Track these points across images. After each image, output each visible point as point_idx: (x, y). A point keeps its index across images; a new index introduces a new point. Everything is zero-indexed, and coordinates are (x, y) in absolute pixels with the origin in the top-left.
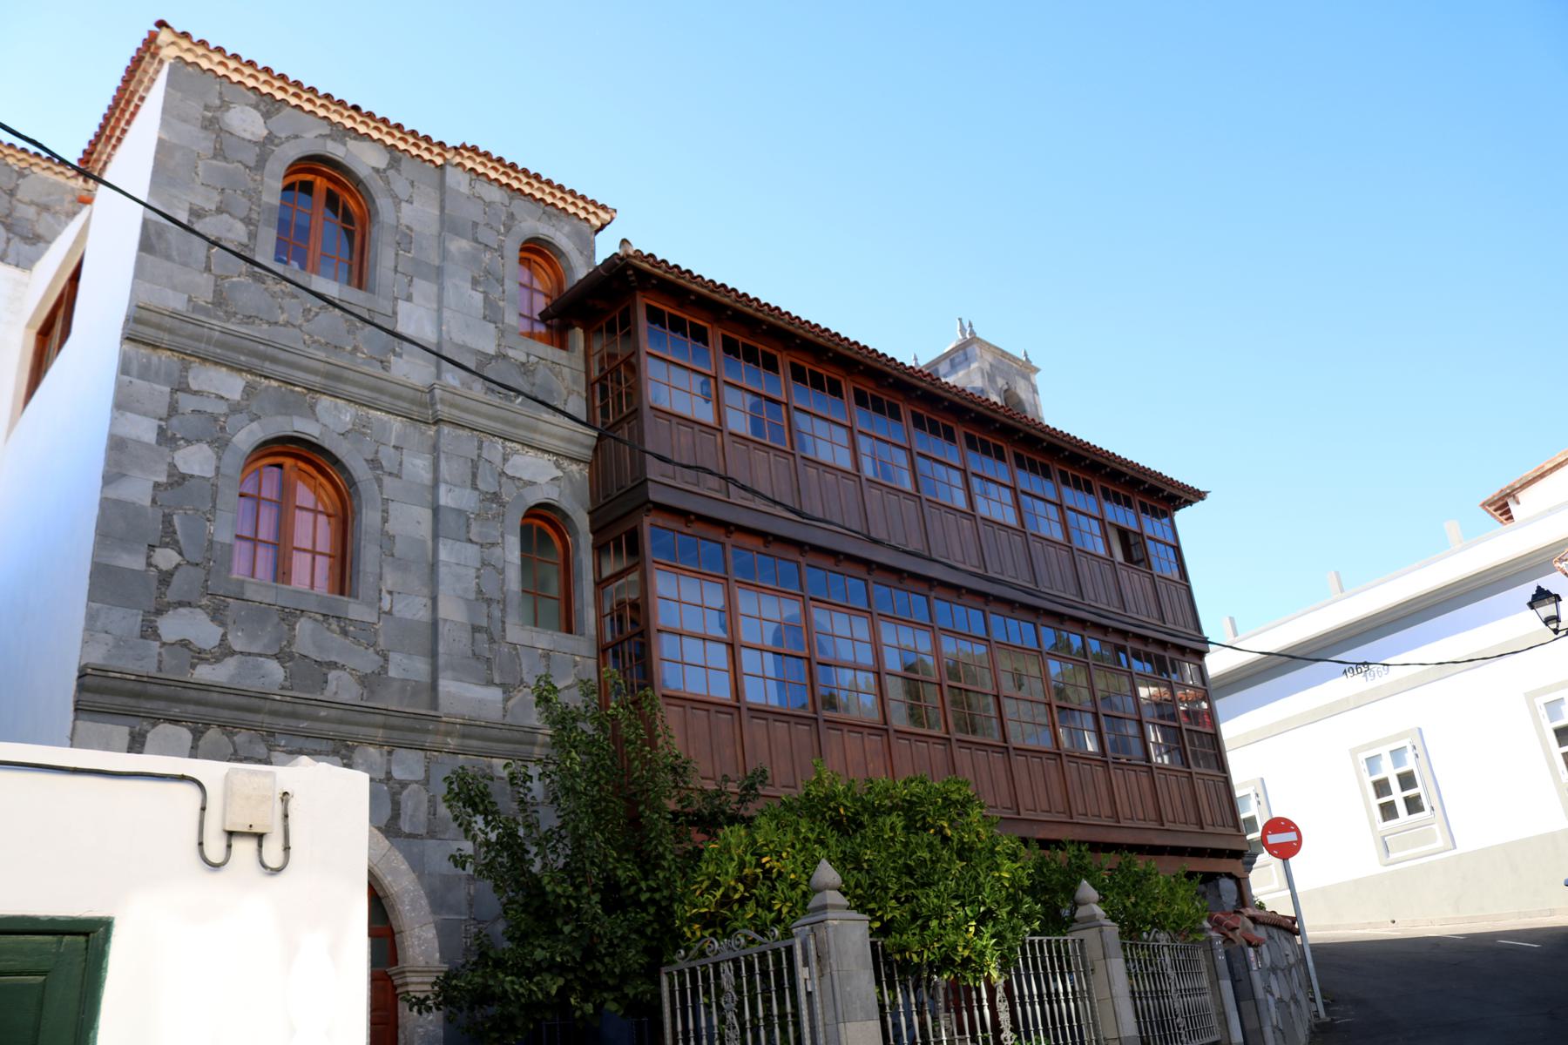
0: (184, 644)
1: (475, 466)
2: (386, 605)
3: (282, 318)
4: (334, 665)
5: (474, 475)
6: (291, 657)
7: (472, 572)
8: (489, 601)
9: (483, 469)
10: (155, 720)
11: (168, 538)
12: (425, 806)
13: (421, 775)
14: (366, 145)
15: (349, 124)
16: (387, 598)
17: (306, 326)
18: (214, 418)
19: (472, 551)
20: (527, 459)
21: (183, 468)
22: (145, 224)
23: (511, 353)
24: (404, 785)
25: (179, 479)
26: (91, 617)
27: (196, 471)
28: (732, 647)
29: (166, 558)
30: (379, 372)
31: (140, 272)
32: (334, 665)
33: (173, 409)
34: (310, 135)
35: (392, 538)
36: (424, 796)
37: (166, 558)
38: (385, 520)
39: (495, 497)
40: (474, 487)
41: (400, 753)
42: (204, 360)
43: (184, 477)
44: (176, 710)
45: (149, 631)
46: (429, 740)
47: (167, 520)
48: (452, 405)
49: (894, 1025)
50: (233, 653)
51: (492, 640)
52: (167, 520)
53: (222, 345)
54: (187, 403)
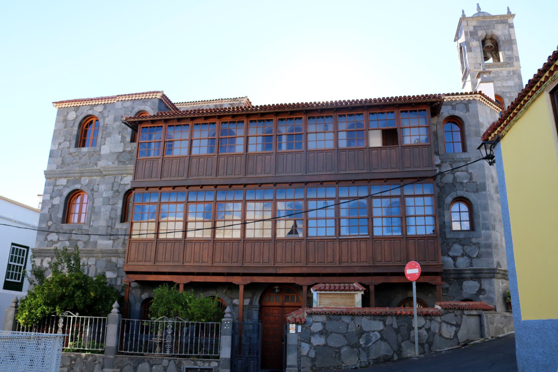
0: (51, 241)
1: (113, 184)
2: (91, 224)
3: (75, 161)
4: (79, 240)
5: (113, 187)
6: (71, 240)
7: (109, 212)
8: (112, 219)
9: (116, 184)
10: (45, 257)
11: (51, 219)
12: (94, 270)
13: (94, 263)
14: (98, 107)
15: (93, 103)
16: (92, 222)
17: (80, 161)
18: (60, 190)
19: (109, 207)
20: (128, 178)
21: (54, 203)
22: (281, 132)
23: (127, 149)
24: (90, 266)
25: (53, 206)
26: (37, 238)
27: (56, 203)
28: (125, 235)
29: (50, 223)
30: (95, 168)
31: (49, 163)
32: (79, 240)
33: (53, 191)
34: (85, 111)
35: (94, 207)
36: (95, 268)
37: (50, 223)
38: (93, 203)
39: (117, 191)
40: (112, 190)
41: (91, 258)
42: (59, 178)
43: (54, 205)
44: (47, 255)
45: (46, 239)
46: (95, 255)
47: (51, 215)
48: (106, 171)
49: (200, 344)
50: (60, 241)
51: (112, 229)
52: (51, 215)
53: (60, 174)
54: (56, 188)
